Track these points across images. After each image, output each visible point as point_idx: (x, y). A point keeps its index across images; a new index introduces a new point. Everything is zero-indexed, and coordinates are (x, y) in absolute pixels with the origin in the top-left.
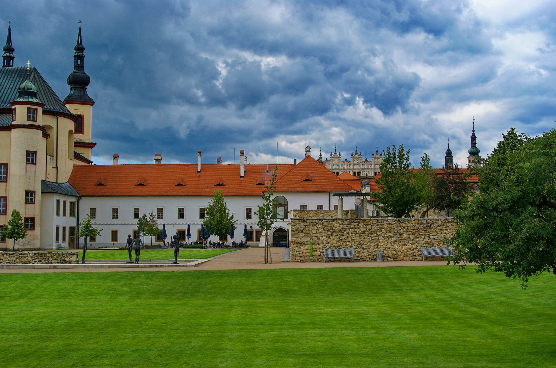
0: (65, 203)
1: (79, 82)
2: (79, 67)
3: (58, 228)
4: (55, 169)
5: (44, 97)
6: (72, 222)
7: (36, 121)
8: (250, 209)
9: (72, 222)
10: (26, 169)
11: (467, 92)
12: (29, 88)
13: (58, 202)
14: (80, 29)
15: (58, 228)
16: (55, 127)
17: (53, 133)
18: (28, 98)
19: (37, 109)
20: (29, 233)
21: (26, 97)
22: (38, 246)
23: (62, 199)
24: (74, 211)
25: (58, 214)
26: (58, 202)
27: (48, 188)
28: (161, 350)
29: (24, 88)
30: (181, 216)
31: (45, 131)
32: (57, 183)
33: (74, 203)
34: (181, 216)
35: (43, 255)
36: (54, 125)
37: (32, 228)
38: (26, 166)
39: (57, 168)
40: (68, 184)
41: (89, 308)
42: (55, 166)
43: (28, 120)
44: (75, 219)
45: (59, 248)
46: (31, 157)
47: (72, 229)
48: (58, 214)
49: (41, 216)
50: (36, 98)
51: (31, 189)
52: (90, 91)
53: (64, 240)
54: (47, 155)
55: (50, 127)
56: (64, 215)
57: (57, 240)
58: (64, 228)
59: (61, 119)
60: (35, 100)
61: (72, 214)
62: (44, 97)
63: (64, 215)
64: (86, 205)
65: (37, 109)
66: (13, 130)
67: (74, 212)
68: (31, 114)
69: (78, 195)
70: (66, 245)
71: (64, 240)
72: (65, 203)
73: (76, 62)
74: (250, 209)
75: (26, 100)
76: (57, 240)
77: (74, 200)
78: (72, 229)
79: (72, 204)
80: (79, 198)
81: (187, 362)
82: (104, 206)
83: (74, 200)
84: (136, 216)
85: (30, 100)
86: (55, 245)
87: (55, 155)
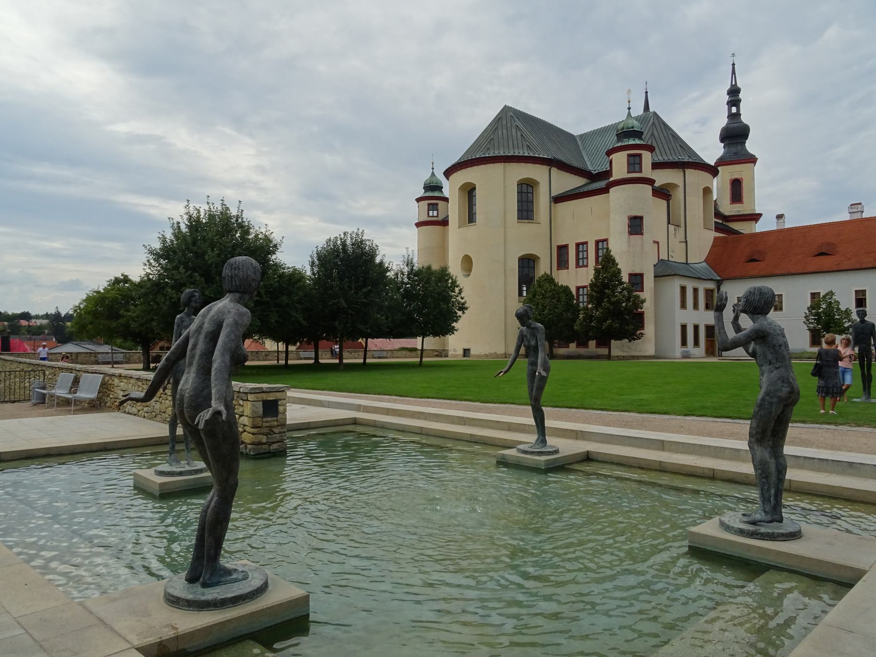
0: (696, 290)
2: (734, 117)
3: (684, 328)
5: (666, 146)
6: (708, 318)
7: (641, 171)
9: (708, 318)
11: (571, 467)
12: (630, 126)
13: (683, 289)
14: (733, 65)
15: (684, 328)
16: (681, 185)
17: (678, 195)
23: (690, 285)
25: (683, 305)
26: (683, 289)
29: (623, 128)
31: (663, 193)
32: (687, 263)
33: (712, 291)
35: (469, 380)
36: (680, 183)
38: (629, 239)
40: (704, 264)
41: (521, 597)
45: (686, 356)
46: (636, 225)
47: (710, 329)
48: (683, 305)
50: (640, 138)
51: (637, 271)
52: (750, 146)
53: (696, 343)
54: (669, 223)
55: (674, 186)
59: (689, 172)
60: (638, 142)
62: (666, 146)
63: (696, 306)
66: (612, 190)
68: (634, 163)
69: (719, 278)
71: (696, 343)
72: (696, 290)
73: (730, 110)
75: (626, 143)
76: (684, 343)
77: (711, 286)
78: (710, 329)
79: (709, 293)
83: (711, 286)
87: (683, 225)
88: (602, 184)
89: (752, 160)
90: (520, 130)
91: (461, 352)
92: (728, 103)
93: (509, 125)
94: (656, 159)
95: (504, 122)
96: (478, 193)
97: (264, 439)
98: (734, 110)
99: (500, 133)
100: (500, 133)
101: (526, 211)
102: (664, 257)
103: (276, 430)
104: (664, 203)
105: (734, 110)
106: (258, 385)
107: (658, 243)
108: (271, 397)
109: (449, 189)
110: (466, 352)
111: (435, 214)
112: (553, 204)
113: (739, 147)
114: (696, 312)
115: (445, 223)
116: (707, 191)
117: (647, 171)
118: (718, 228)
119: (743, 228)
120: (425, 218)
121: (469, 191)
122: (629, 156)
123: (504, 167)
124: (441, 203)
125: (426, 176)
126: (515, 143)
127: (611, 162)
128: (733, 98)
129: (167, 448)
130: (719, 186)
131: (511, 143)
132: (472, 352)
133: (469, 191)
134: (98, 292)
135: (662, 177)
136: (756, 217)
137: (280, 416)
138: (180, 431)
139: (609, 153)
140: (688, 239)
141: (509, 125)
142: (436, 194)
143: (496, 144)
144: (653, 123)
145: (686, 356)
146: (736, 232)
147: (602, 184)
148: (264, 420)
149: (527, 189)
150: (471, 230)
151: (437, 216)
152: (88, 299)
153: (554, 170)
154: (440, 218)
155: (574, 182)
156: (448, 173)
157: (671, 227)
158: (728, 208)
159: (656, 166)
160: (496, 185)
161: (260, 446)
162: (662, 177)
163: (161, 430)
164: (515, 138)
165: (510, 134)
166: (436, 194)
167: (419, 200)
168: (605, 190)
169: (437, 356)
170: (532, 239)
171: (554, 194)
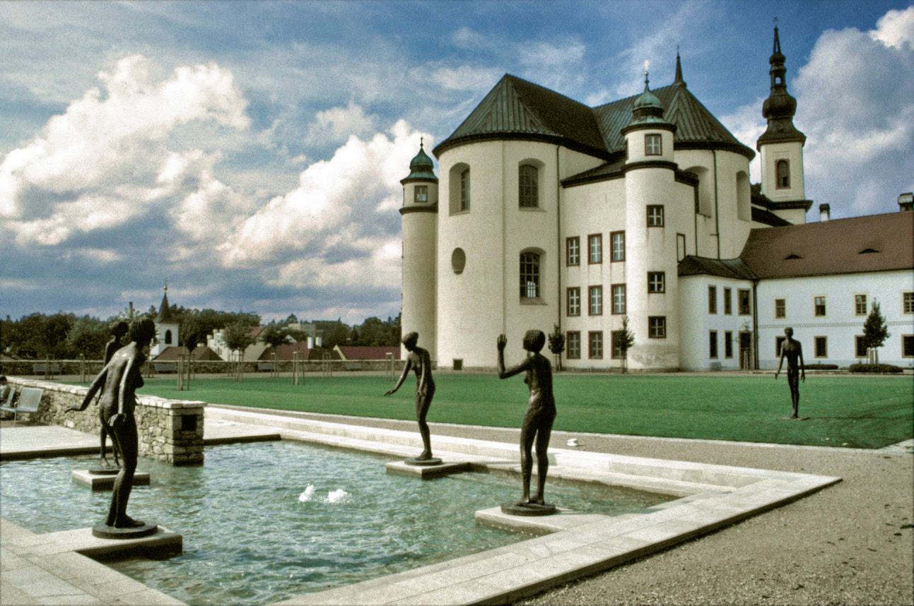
0: (728, 292)
3: (713, 336)
4: (715, 238)
7: (661, 155)
8: (864, 297)
10: (611, 267)
12: (648, 101)
13: (712, 290)
14: (776, 30)
15: (713, 336)
17: (707, 181)
18: (646, 119)
21: (642, 118)
23: (721, 284)
24: (747, 303)
25: (713, 309)
26: (712, 290)
28: (412, 521)
29: (640, 105)
30: (821, 310)
31: (689, 178)
33: (747, 292)
34: (821, 310)
38: (648, 232)
39: (718, 235)
42: (715, 232)
43: (647, 154)
44: (619, 318)
45: (716, 368)
46: (655, 215)
48: (713, 309)
53: (729, 353)
54: (697, 211)
56: (728, 310)
57: (713, 353)
59: (721, 154)
63: (728, 310)
64: (768, 292)
65: (660, 135)
71: (729, 353)
72: (728, 292)
74: (864, 297)
76: (713, 353)
77: (746, 285)
80: (755, 281)
82: (799, 293)
84: (861, 308)
89: (800, 138)
91: (451, 364)
92: (771, 73)
94: (677, 139)
96: (473, 175)
98: (778, 81)
100: (499, 104)
101: (528, 197)
102: (691, 251)
104: (690, 190)
105: (778, 81)
106: (203, 361)
107: (684, 236)
108: (190, 413)
109: (442, 169)
110: (458, 364)
111: (424, 199)
112: (561, 188)
113: (786, 122)
114: (728, 317)
115: (433, 209)
116: (742, 176)
117: (668, 153)
118: (757, 216)
119: (794, 217)
120: (410, 202)
121: (461, 173)
122: (647, 136)
123: (503, 145)
124: (429, 185)
125: (414, 153)
128: (776, 68)
129: (99, 456)
130: (758, 170)
132: (465, 364)
133: (461, 173)
134: (234, 314)
135: (686, 160)
136: (805, 205)
138: (109, 443)
139: (624, 132)
140: (721, 231)
142: (425, 175)
145: (716, 368)
146: (784, 223)
149: (529, 172)
150: (460, 218)
151: (426, 202)
152: (210, 310)
153: (563, 150)
154: (429, 203)
156: (438, 151)
157: (700, 218)
158: (773, 193)
159: (678, 146)
160: (492, 165)
162: (686, 160)
163: (94, 441)
166: (425, 175)
167: (403, 182)
168: (621, 174)
171: (563, 177)
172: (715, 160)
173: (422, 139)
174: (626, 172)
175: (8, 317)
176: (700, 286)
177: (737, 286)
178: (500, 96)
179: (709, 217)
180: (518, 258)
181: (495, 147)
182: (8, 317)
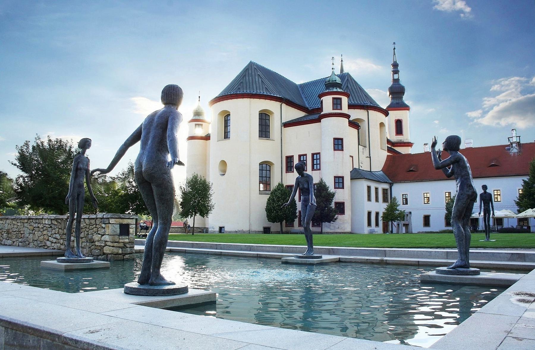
0: (377, 189)
1: (397, 91)
3: (369, 214)
4: (369, 159)
5: (356, 94)
10: (334, 155)
12: (334, 80)
13: (369, 188)
15: (369, 214)
17: (364, 126)
19: (340, 99)
20: (340, 217)
22: (348, 229)
23: (373, 185)
25: (369, 199)
26: (369, 188)
27: (357, 175)
29: (329, 81)
32: (371, 171)
33: (387, 190)
37: (342, 212)
39: (370, 157)
40: (381, 172)
45: (371, 232)
46: (338, 144)
48: (369, 199)
49: (352, 200)
53: (377, 225)
54: (359, 144)
55: (361, 120)
57: (369, 224)
58: (377, 214)
59: (371, 112)
61: (385, 200)
63: (377, 200)
67: (387, 198)
68: (337, 103)
69: (391, 182)
70: (379, 230)
72: (377, 189)
76: (369, 224)
77: (386, 186)
79: (385, 191)
80: (391, 185)
81: (228, 305)
83: (386, 186)
85: (335, 90)
86: (366, 230)
88: (316, 116)
90: (261, 78)
93: (253, 74)
94: (350, 102)
95: (250, 72)
97: (120, 252)
99: (247, 78)
100: (247, 78)
101: (264, 131)
103: (127, 245)
104: (355, 131)
107: (352, 157)
110: (221, 229)
117: (345, 109)
122: (333, 98)
123: (250, 102)
126: (258, 85)
127: (322, 102)
131: (255, 85)
132: (227, 229)
137: (130, 235)
139: (321, 96)
141: (253, 74)
143: (245, 85)
144: (348, 80)
147: (316, 116)
148: (120, 237)
153: (284, 105)
155: (298, 114)
161: (117, 256)
164: (257, 83)
165: (254, 81)
168: (318, 120)
169: (200, 232)
170: (269, 151)
171: (284, 121)
172: (358, 133)
173: (394, 49)
174: (158, 266)
175: (85, 144)
176: (363, 185)
177: (382, 186)
178: (247, 73)
179: (365, 147)
180: (257, 168)
181: (246, 101)
182: (85, 144)
